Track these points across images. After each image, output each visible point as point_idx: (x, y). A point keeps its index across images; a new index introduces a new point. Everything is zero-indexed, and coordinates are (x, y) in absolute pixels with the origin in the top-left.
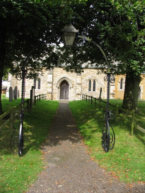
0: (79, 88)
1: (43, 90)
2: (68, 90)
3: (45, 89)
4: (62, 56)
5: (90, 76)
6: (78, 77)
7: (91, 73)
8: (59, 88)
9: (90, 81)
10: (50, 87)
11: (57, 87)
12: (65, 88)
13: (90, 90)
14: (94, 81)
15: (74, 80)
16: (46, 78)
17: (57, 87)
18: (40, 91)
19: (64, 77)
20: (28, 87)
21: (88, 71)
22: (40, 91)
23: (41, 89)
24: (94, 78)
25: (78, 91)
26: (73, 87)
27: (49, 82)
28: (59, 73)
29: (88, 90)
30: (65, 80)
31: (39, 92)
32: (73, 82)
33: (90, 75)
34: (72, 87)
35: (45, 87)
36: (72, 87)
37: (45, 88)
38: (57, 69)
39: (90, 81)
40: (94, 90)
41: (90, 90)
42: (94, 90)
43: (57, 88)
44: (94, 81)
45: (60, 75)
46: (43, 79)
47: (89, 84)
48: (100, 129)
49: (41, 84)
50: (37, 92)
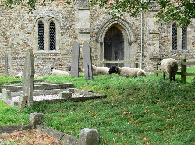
0: (154, 42)
1: (65, 52)
2: (122, 49)
6: (151, 17)
8: (101, 45)
9: (41, 26)
11: (97, 42)
12: (113, 46)
13: (42, 47)
15: (137, 25)
16: (70, 19)
17: (97, 42)
18: (56, 54)
20: (23, 45)
23: (58, 50)
25: (153, 50)
26: (138, 42)
27: (82, 30)
29: (171, 48)
30: (116, 23)
31: (54, 57)
32: (136, 27)
36: (135, 42)
39: (41, 26)
42: (184, 46)
43: (99, 45)
46: (62, 23)
47: (173, 34)
50: (48, 59)
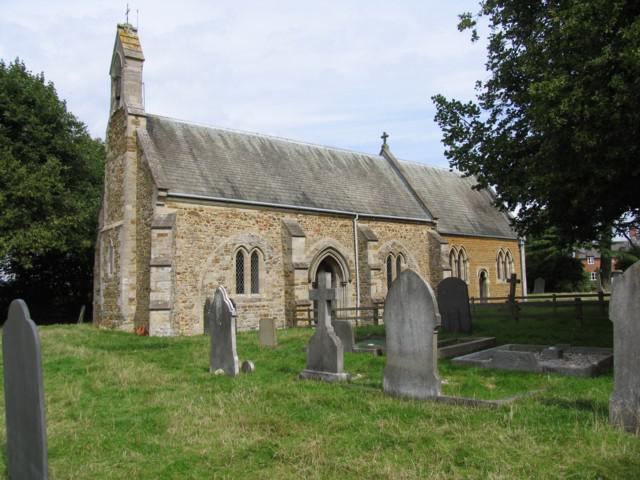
3: (276, 290)
4: (544, 193)
5: (390, 243)
7: (390, 234)
9: (240, 255)
10: (303, 283)
14: (255, 256)
18: (260, 300)
19: (331, 248)
21: (383, 229)
22: (260, 300)
24: (399, 250)
26: (354, 281)
28: (312, 233)
31: (258, 304)
33: (389, 239)
34: (350, 281)
35: (275, 283)
37: (274, 286)
38: (304, 220)
40: (255, 290)
41: (240, 289)
42: (255, 290)
44: (255, 256)
45: (315, 241)
46: (266, 254)
48: (476, 369)
49: (262, 275)
